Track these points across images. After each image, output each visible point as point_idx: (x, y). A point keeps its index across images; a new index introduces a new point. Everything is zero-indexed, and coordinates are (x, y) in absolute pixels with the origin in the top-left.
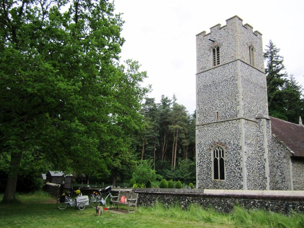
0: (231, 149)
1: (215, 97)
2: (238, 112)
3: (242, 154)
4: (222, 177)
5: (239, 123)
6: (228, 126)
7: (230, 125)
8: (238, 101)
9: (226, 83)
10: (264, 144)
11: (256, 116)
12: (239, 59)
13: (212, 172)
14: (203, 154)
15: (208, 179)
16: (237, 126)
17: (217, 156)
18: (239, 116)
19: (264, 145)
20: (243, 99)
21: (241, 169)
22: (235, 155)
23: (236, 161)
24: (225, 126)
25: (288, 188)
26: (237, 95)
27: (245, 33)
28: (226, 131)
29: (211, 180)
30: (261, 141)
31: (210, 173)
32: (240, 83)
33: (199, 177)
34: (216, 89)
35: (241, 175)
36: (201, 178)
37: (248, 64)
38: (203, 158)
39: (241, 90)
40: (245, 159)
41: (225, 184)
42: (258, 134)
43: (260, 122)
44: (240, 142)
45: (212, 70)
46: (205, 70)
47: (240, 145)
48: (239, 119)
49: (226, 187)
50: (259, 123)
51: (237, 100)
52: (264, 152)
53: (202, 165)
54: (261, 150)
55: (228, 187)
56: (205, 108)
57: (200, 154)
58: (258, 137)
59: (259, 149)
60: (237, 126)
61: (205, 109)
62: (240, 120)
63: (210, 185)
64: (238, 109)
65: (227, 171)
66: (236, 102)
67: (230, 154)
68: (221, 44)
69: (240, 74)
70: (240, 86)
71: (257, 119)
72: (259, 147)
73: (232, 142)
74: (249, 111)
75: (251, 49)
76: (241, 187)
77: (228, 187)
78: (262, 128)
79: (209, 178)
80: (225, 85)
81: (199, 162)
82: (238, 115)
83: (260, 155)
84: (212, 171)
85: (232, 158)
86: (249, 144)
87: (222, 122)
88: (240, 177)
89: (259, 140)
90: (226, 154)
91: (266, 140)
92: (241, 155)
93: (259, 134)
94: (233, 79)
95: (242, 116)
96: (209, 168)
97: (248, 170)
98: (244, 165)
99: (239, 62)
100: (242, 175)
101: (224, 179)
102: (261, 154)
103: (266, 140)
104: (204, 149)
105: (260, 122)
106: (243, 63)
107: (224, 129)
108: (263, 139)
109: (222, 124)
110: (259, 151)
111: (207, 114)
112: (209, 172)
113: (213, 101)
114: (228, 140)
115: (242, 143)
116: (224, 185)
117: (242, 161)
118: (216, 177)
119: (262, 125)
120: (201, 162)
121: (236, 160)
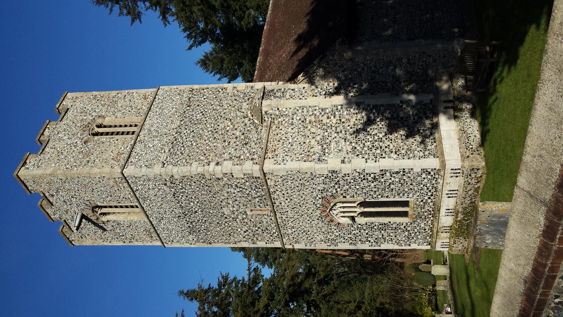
0: (336, 189)
1: (214, 214)
2: (250, 177)
3: (347, 168)
4: (405, 204)
5: (275, 174)
6: (283, 194)
7: (280, 190)
8: (221, 176)
9: (182, 196)
10: (322, 106)
11: (256, 121)
12: (120, 171)
13: (392, 223)
14: (350, 236)
15: (409, 229)
16: (281, 177)
17: (355, 212)
18: (257, 174)
19: (324, 107)
20: (217, 164)
21: (383, 172)
22: (350, 183)
23: (364, 181)
24: (282, 199)
25: (423, 53)
26: (208, 177)
27: (59, 146)
28: (295, 196)
29: (411, 224)
30: (315, 112)
31: (394, 226)
32: (177, 171)
33: (403, 245)
34: (196, 212)
35: (397, 173)
36: (406, 241)
37: (135, 143)
38: (360, 237)
39: (196, 168)
40: (358, 163)
41: (420, 200)
42: (300, 119)
43: (271, 115)
44: (318, 172)
45: (152, 220)
46: (152, 230)
47: (326, 172)
48: (264, 174)
49: (426, 198)
50: (273, 116)
51: (220, 176)
52: (339, 107)
53: (376, 239)
54: (337, 113)
55: (427, 195)
56: (242, 232)
57: (351, 241)
58: (305, 119)
59: (334, 117)
60: (281, 177)
61: (245, 232)
62: (266, 170)
63: (422, 225)
64: (243, 176)
65: (387, 197)
66: (225, 179)
67: (348, 190)
68: (88, 203)
69: (157, 169)
70: (187, 171)
71: (262, 120)
72: (328, 118)
73: (321, 187)
74: (246, 144)
75: (101, 130)
76: (427, 171)
77: (427, 195)
78: (284, 110)
79: (405, 227)
80: (187, 197)
81: (367, 243)
82: (254, 176)
83: (347, 117)
84: (390, 222)
85: (358, 187)
86: (323, 150)
87: (273, 204)
88: (401, 173)
89: (313, 117)
90: (348, 197)
91: (311, 101)
92: (350, 172)
93: (298, 118)
94: (172, 183)
95: (257, 167)
96: (380, 226)
97: (384, 155)
98: (373, 167)
99: (126, 172)
100: (398, 170)
101: (408, 201)
102: (345, 113)
103: (311, 101)
104: (337, 234)
105: (271, 115)
106: (131, 159)
107: (289, 200)
108: (310, 109)
109: (277, 204)
110: (337, 118)
111: (257, 228)
112: (392, 228)
113: (226, 218)
114: (314, 193)
115: (322, 168)
116: (422, 201)
117: (364, 170)
118: (405, 214)
119: (278, 109)
120: (369, 241)
121: (362, 181)
